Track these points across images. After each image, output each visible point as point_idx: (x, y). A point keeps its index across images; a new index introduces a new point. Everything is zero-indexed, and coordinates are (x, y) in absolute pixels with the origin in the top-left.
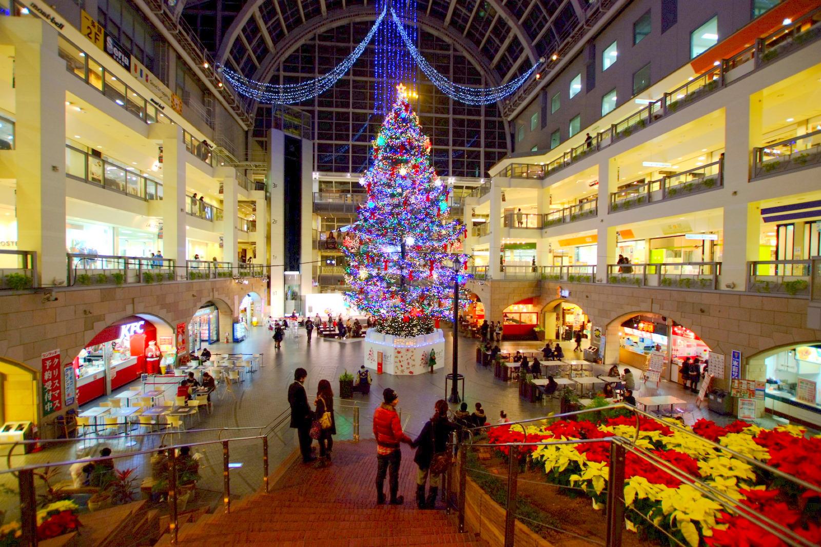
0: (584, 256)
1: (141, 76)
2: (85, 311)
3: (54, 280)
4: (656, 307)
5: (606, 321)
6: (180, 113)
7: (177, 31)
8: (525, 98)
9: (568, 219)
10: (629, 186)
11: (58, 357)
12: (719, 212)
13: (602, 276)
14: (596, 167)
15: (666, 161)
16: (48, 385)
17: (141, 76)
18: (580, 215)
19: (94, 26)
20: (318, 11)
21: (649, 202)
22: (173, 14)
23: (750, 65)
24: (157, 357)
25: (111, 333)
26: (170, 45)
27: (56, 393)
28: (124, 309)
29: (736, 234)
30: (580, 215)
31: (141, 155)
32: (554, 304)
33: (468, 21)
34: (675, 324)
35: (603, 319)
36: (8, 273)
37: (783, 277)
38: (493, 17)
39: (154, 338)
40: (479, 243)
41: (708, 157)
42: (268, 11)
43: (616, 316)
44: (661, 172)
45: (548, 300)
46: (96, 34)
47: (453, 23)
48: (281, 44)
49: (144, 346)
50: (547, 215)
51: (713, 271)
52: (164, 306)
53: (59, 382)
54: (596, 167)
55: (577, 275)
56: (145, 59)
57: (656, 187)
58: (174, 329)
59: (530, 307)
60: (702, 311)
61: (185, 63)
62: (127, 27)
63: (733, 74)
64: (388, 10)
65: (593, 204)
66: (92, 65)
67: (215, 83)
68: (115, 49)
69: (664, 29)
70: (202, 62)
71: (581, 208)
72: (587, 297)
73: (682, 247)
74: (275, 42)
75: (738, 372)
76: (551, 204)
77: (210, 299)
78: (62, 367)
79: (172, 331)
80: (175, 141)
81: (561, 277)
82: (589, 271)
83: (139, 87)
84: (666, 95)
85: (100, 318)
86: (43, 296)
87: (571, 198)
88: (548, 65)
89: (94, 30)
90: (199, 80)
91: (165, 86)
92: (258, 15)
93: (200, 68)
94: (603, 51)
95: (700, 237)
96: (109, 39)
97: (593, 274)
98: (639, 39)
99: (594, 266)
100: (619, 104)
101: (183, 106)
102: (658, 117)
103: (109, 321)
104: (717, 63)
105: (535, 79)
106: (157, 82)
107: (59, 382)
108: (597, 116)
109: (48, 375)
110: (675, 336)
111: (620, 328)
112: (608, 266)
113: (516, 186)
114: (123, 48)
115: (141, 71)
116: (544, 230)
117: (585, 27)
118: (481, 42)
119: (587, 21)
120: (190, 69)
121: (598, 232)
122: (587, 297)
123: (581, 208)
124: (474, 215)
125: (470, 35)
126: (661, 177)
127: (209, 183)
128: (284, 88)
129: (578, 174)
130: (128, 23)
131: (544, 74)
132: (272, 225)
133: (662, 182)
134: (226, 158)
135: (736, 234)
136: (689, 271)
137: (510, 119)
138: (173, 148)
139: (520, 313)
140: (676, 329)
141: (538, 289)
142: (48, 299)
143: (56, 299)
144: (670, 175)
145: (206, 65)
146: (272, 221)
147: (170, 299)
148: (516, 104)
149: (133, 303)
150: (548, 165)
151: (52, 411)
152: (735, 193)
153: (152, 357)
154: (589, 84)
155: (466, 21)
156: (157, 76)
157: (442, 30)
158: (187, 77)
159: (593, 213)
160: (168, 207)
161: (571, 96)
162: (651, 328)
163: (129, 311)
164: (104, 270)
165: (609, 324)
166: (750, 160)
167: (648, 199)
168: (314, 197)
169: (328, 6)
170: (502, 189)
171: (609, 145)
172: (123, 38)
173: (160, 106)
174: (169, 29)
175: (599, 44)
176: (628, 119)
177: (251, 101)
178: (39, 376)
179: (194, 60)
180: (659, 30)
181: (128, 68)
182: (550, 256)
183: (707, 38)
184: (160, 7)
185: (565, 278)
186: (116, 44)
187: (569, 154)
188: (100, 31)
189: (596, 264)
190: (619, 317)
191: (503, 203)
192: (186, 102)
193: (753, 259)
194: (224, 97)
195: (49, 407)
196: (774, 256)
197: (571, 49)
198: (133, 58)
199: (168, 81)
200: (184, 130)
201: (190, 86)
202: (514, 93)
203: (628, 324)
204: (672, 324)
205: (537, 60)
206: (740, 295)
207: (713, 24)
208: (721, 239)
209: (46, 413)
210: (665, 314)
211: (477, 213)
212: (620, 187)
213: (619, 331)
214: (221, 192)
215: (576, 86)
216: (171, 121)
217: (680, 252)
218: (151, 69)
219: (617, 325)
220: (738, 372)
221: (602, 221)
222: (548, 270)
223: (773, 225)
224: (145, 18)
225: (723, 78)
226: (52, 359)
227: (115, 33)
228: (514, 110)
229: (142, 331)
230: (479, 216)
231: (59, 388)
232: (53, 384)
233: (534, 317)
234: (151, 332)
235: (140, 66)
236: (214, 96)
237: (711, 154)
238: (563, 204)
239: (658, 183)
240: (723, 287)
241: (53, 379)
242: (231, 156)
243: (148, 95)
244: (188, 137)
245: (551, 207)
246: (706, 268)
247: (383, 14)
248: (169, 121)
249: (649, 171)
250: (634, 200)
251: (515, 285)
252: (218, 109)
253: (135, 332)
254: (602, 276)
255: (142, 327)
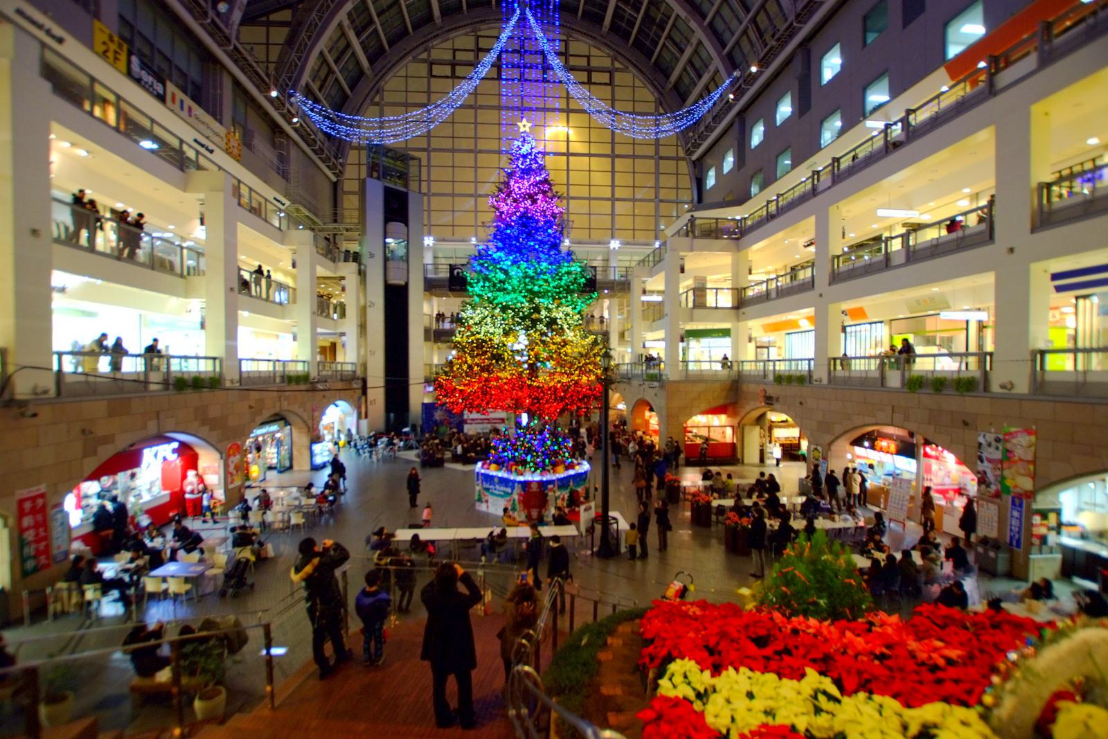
0: (791, 344)
1: (182, 108)
2: (83, 431)
3: (35, 388)
4: (898, 417)
5: (828, 438)
6: (238, 159)
7: (232, 47)
8: (715, 128)
9: (773, 295)
10: (860, 246)
11: (42, 496)
12: (989, 279)
13: (821, 374)
14: (812, 219)
15: (911, 209)
16: (30, 535)
17: (182, 108)
18: (793, 289)
19: (112, 40)
20: (430, 18)
21: (887, 266)
22: (227, 25)
23: (1031, 62)
24: (199, 492)
25: (128, 460)
26: (223, 67)
27: (42, 546)
28: (144, 427)
29: (1013, 310)
30: (793, 289)
31: (181, 217)
32: (756, 414)
33: (634, 24)
34: (927, 443)
35: (825, 431)
36: (192, 375)
37: (1085, 372)
38: (669, 18)
39: (195, 467)
40: (652, 331)
41: (971, 201)
42: (362, 22)
43: (842, 431)
44: (904, 225)
45: (748, 408)
46: (116, 52)
47: (614, 28)
48: (378, 64)
49: (180, 477)
50: (745, 289)
51: (982, 363)
52: (205, 421)
53: (46, 531)
54: (812, 219)
55: (787, 374)
56: (190, 87)
57: (896, 245)
58: (221, 453)
59: (722, 419)
60: (966, 424)
61: (245, 92)
62: (163, 44)
63: (1005, 77)
64: (523, 13)
65: (808, 273)
66: (99, 90)
67: (288, 117)
68: (143, 72)
69: (906, 22)
70: (269, 90)
71: (794, 278)
72: (801, 404)
73: (937, 331)
74: (372, 61)
75: (1020, 528)
76: (750, 273)
77: (277, 410)
78: (49, 508)
79: (217, 455)
80: (221, 195)
81: (765, 376)
82: (804, 366)
83: (176, 123)
84: (909, 112)
85: (108, 439)
86: (16, 411)
87: (779, 265)
88: (745, 81)
89: (113, 47)
90: (266, 114)
91: (218, 124)
92: (346, 23)
93: (265, 97)
94: (821, 58)
95: (962, 316)
96: (134, 59)
97: (810, 370)
98: (871, 37)
99: (809, 360)
100: (842, 132)
101: (244, 152)
102: (897, 145)
103: (121, 444)
104: (982, 64)
105: (728, 101)
106: (208, 119)
107: (46, 531)
108: (814, 147)
109: (27, 521)
110: (927, 460)
111: (848, 447)
112: (829, 360)
113: (702, 249)
114: (154, 70)
115: (182, 102)
116: (742, 311)
117: (795, 24)
118: (653, 52)
119: (798, 16)
120: (253, 100)
121: (816, 312)
122: (801, 404)
123: (794, 278)
124: (644, 292)
125: (638, 44)
126: (903, 231)
127: (281, 256)
128: (380, 122)
129: (788, 230)
130: (164, 40)
131: (739, 93)
132: (369, 310)
133: (905, 237)
134: (306, 220)
135: (1013, 310)
136: (947, 365)
137: (694, 157)
138: (219, 201)
139: (709, 427)
140: (928, 449)
141: (733, 393)
142: (22, 415)
143: (35, 415)
144: (917, 228)
145: (274, 94)
146: (368, 304)
147: (214, 412)
148: (702, 137)
149: (158, 418)
150: (745, 219)
151: (36, 569)
152: (1011, 250)
153: (192, 492)
154: (802, 106)
155: (632, 24)
156: (207, 111)
157: (599, 38)
158: (250, 111)
159: (810, 285)
160: (215, 284)
161: (778, 123)
162: (893, 448)
163: (152, 428)
164: (183, 373)
165: (833, 442)
166: (1032, 202)
167: (887, 263)
168: (425, 271)
169: (444, 13)
170: (682, 254)
171: (829, 188)
172: (158, 58)
173: (207, 149)
174: (220, 45)
175: (815, 46)
176: (793, 188)
177: (340, 143)
178: (11, 521)
179: (258, 87)
180: (900, 23)
181: (161, 98)
182: (751, 346)
183: (969, 30)
184: (206, 14)
185: (771, 377)
186: (144, 66)
187: (774, 203)
188: (120, 46)
189: (812, 355)
190: (846, 432)
191: (681, 275)
192: (247, 143)
193: (1041, 345)
194: (302, 137)
195: (30, 564)
196: (1072, 342)
197: (776, 56)
198: (169, 84)
199: (221, 115)
200: (239, 181)
201: (254, 122)
202: (697, 123)
203: (858, 442)
204: (922, 441)
205: (730, 75)
206: (1021, 398)
207: (978, 11)
208: (992, 319)
209: (25, 574)
210: (913, 427)
211: (649, 288)
212: (850, 247)
213: (846, 452)
214: (294, 266)
215: (785, 110)
216: (220, 168)
217: (934, 338)
218: (196, 99)
219: (843, 444)
220: (1020, 528)
221: (821, 295)
222: (747, 367)
223: (1069, 296)
224: (188, 33)
225: (991, 83)
226: (33, 499)
227: (146, 51)
228: (700, 145)
229: (176, 455)
230: (652, 292)
231: (46, 538)
232: (37, 535)
233: (729, 431)
234: (189, 457)
235: (180, 95)
236: (288, 136)
237: (976, 196)
238: (769, 273)
239: (900, 240)
240: (995, 388)
241: (37, 526)
242: (313, 217)
243: (188, 134)
244: (244, 191)
245: (750, 277)
246: (972, 361)
247: (515, 18)
248: (217, 168)
249: (886, 224)
250: (871, 264)
251: (701, 387)
252: (293, 152)
253: (165, 459)
254: (821, 374)
255: (174, 451)
